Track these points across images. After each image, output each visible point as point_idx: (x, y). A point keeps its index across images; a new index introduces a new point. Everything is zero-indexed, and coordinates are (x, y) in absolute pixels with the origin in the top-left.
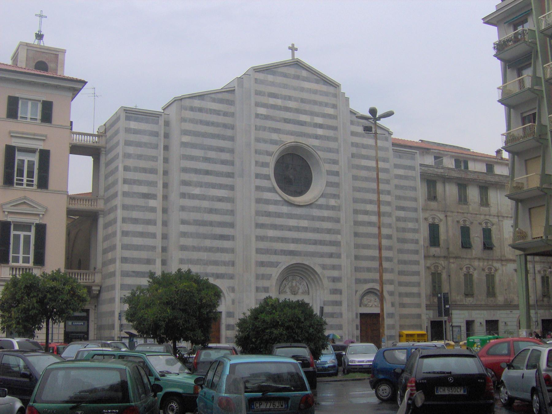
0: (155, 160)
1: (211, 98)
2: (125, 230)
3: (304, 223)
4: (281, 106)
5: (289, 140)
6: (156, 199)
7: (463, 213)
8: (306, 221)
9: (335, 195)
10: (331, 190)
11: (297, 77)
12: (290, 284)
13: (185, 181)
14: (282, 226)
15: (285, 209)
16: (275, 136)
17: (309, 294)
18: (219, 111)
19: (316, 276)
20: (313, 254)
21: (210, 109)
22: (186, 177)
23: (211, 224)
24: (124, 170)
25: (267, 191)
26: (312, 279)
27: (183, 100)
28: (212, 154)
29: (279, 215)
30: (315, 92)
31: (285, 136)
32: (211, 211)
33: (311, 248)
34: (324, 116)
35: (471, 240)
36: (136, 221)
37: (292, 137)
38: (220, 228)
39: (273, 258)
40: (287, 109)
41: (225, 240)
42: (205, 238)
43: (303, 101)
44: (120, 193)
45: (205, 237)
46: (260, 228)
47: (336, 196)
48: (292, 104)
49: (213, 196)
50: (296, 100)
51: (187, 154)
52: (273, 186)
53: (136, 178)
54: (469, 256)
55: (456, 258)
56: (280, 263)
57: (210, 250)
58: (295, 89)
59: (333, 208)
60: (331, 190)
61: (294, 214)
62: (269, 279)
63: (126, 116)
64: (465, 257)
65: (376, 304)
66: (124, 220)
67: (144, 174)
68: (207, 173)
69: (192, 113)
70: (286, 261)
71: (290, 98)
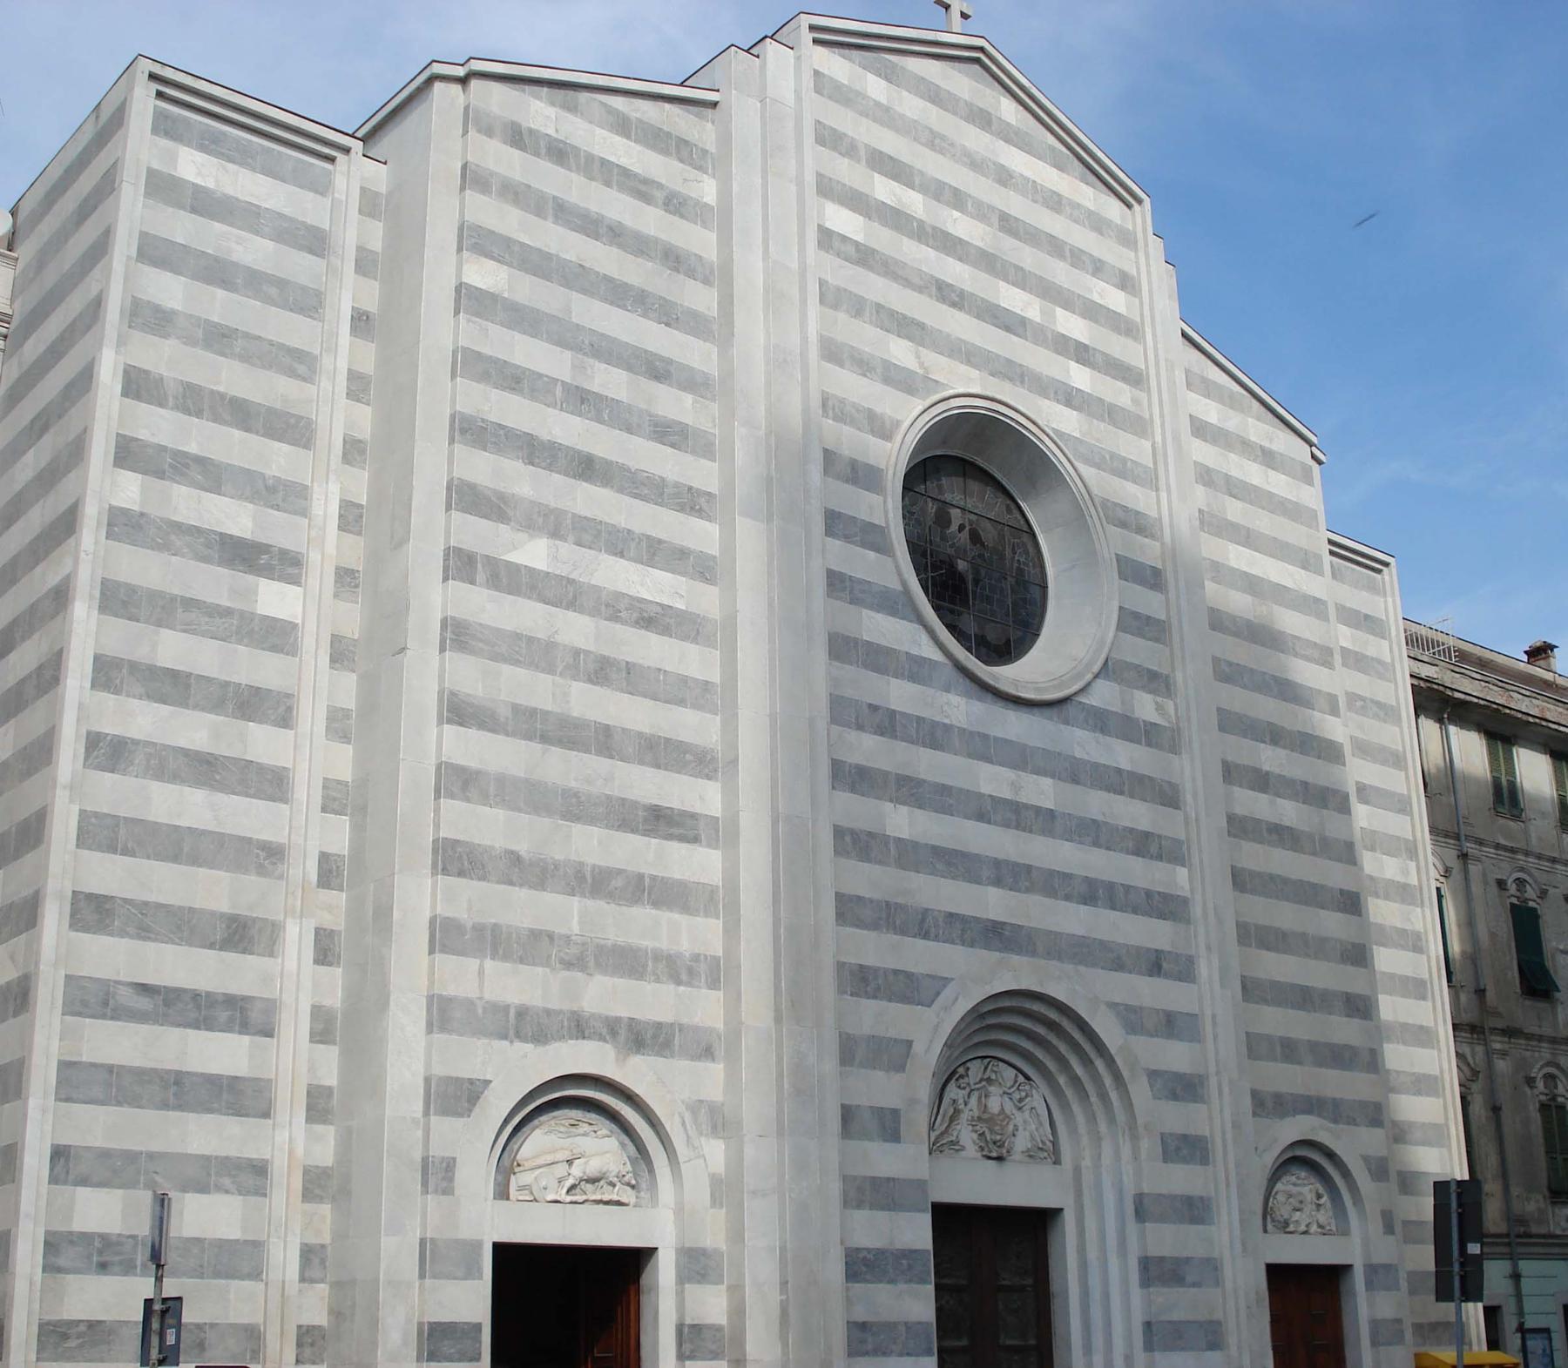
0: (301, 369)
1: (610, 110)
2: (109, 728)
3: (1041, 791)
4: (921, 223)
5: (963, 385)
6: (295, 581)
7: (1512, 850)
8: (1046, 783)
9: (1153, 676)
10: (1139, 651)
11: (983, 119)
12: (973, 1101)
13: (472, 487)
14: (944, 790)
15: (959, 709)
16: (901, 352)
17: (1057, 1162)
18: (646, 181)
19: (1100, 1064)
20: (1084, 951)
21: (604, 162)
22: (482, 468)
23: (604, 741)
24: (126, 393)
25: (879, 608)
26: (1075, 1081)
27: (474, 84)
28: (610, 381)
29: (933, 735)
30: (1055, 202)
31: (943, 361)
32: (602, 671)
33: (1073, 919)
34: (1092, 312)
35: (1549, 964)
36: (173, 687)
37: (975, 373)
38: (650, 772)
39: (918, 956)
40: (949, 244)
41: (670, 837)
42: (577, 819)
43: (1008, 224)
44: (91, 513)
45: (574, 807)
46: (853, 790)
47: (1156, 682)
48: (962, 226)
49: (619, 596)
50: (982, 212)
51: (487, 350)
52: (904, 583)
53: (193, 448)
54: (1547, 1031)
55: (1511, 1033)
56: (946, 981)
57: (594, 882)
58: (976, 164)
59: (1148, 735)
60: (1139, 651)
61: (996, 739)
62: (901, 1068)
63: (159, 116)
64: (1535, 1030)
65: (1322, 1217)
66: (107, 673)
67: (237, 434)
68: (586, 468)
69: (516, 153)
70: (977, 976)
71: (958, 200)
